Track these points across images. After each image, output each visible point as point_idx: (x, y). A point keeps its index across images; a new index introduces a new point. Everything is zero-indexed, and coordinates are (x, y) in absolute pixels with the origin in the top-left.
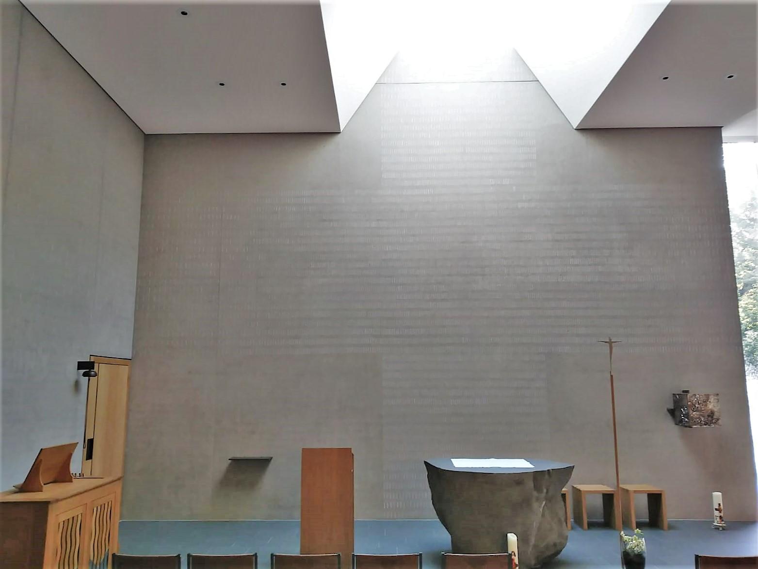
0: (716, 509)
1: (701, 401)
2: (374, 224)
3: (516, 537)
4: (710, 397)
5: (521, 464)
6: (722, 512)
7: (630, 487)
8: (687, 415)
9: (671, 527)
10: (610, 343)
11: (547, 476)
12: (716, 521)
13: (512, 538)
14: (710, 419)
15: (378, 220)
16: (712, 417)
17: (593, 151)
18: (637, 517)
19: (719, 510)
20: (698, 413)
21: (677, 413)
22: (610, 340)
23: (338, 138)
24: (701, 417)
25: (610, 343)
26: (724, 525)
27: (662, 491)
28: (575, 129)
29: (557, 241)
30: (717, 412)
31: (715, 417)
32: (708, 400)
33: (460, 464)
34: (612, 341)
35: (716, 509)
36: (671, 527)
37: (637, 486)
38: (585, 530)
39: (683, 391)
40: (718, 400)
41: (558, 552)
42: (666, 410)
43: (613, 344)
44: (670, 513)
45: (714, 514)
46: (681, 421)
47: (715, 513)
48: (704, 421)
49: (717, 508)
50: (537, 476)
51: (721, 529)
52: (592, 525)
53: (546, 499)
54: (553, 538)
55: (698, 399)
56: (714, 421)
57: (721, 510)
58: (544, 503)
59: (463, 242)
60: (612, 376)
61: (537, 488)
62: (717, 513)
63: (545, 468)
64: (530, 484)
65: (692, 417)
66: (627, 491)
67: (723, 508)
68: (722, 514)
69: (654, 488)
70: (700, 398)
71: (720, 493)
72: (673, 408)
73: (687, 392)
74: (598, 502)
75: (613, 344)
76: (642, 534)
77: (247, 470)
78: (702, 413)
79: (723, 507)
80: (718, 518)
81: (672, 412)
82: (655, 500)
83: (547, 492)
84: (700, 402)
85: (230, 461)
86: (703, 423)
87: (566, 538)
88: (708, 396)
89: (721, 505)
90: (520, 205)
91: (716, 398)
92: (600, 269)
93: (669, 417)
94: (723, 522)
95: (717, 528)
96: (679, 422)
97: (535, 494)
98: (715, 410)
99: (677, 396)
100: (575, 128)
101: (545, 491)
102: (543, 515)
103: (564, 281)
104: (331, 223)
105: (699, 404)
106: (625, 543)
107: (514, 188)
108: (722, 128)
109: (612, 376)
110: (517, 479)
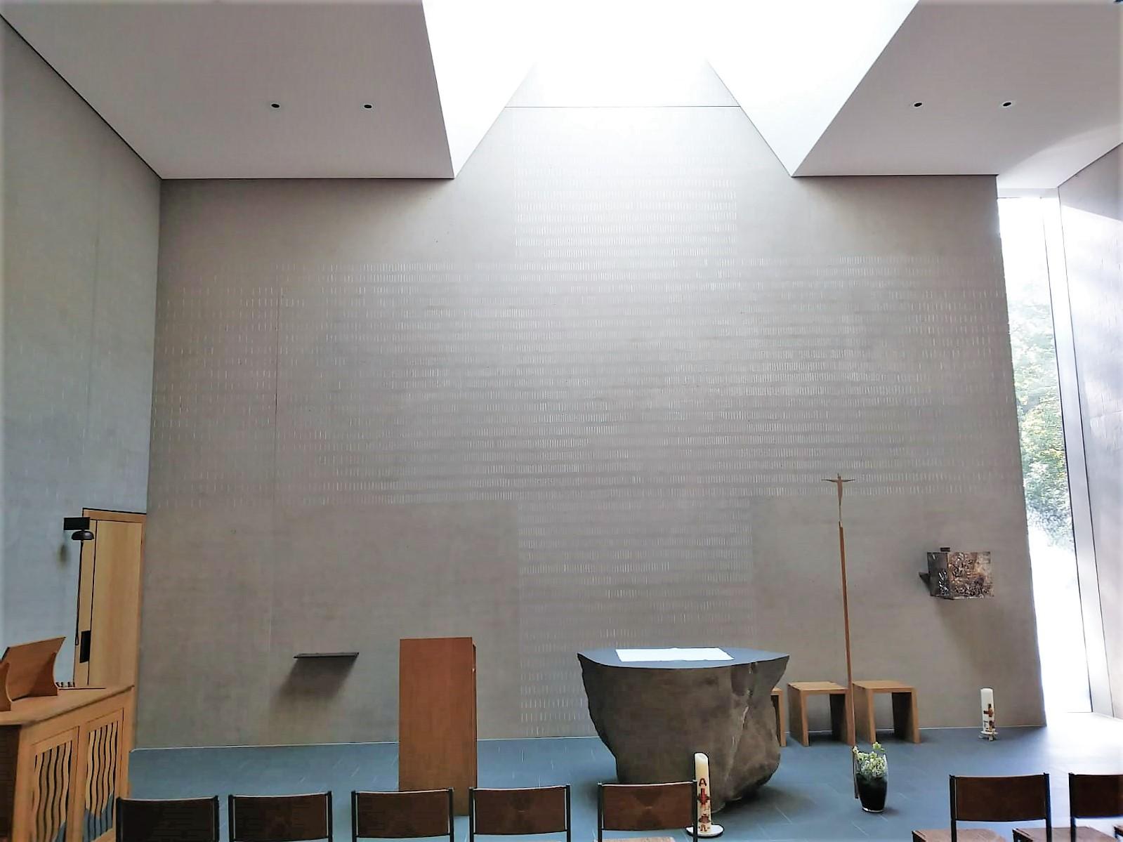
0: (985, 712)
5: (715, 656)
8: (947, 583)
9: (923, 739)
10: (840, 482)
12: (985, 729)
13: (701, 759)
14: (978, 586)
15: (511, 308)
16: (981, 585)
17: (818, 209)
19: (989, 713)
22: (839, 478)
25: (840, 482)
26: (995, 733)
28: (792, 177)
31: (985, 584)
33: (629, 656)
35: (985, 712)
37: (878, 683)
39: (941, 549)
40: (989, 560)
44: (922, 719)
46: (939, 591)
50: (737, 671)
51: (991, 739)
52: (814, 739)
54: (759, 758)
55: (963, 559)
60: (841, 529)
61: (737, 689)
62: (986, 717)
64: (727, 683)
65: (954, 586)
68: (993, 719)
71: (991, 690)
73: (947, 549)
77: (321, 672)
80: (988, 724)
81: (926, 578)
82: (902, 701)
83: (751, 694)
84: (964, 564)
85: (296, 659)
89: (992, 706)
90: (713, 286)
91: (986, 557)
94: (994, 730)
95: (986, 738)
96: (936, 593)
97: (734, 696)
98: (986, 574)
100: (791, 175)
101: (748, 692)
106: (858, 763)
107: (706, 261)
108: (997, 177)
109: (841, 529)
110: (708, 676)
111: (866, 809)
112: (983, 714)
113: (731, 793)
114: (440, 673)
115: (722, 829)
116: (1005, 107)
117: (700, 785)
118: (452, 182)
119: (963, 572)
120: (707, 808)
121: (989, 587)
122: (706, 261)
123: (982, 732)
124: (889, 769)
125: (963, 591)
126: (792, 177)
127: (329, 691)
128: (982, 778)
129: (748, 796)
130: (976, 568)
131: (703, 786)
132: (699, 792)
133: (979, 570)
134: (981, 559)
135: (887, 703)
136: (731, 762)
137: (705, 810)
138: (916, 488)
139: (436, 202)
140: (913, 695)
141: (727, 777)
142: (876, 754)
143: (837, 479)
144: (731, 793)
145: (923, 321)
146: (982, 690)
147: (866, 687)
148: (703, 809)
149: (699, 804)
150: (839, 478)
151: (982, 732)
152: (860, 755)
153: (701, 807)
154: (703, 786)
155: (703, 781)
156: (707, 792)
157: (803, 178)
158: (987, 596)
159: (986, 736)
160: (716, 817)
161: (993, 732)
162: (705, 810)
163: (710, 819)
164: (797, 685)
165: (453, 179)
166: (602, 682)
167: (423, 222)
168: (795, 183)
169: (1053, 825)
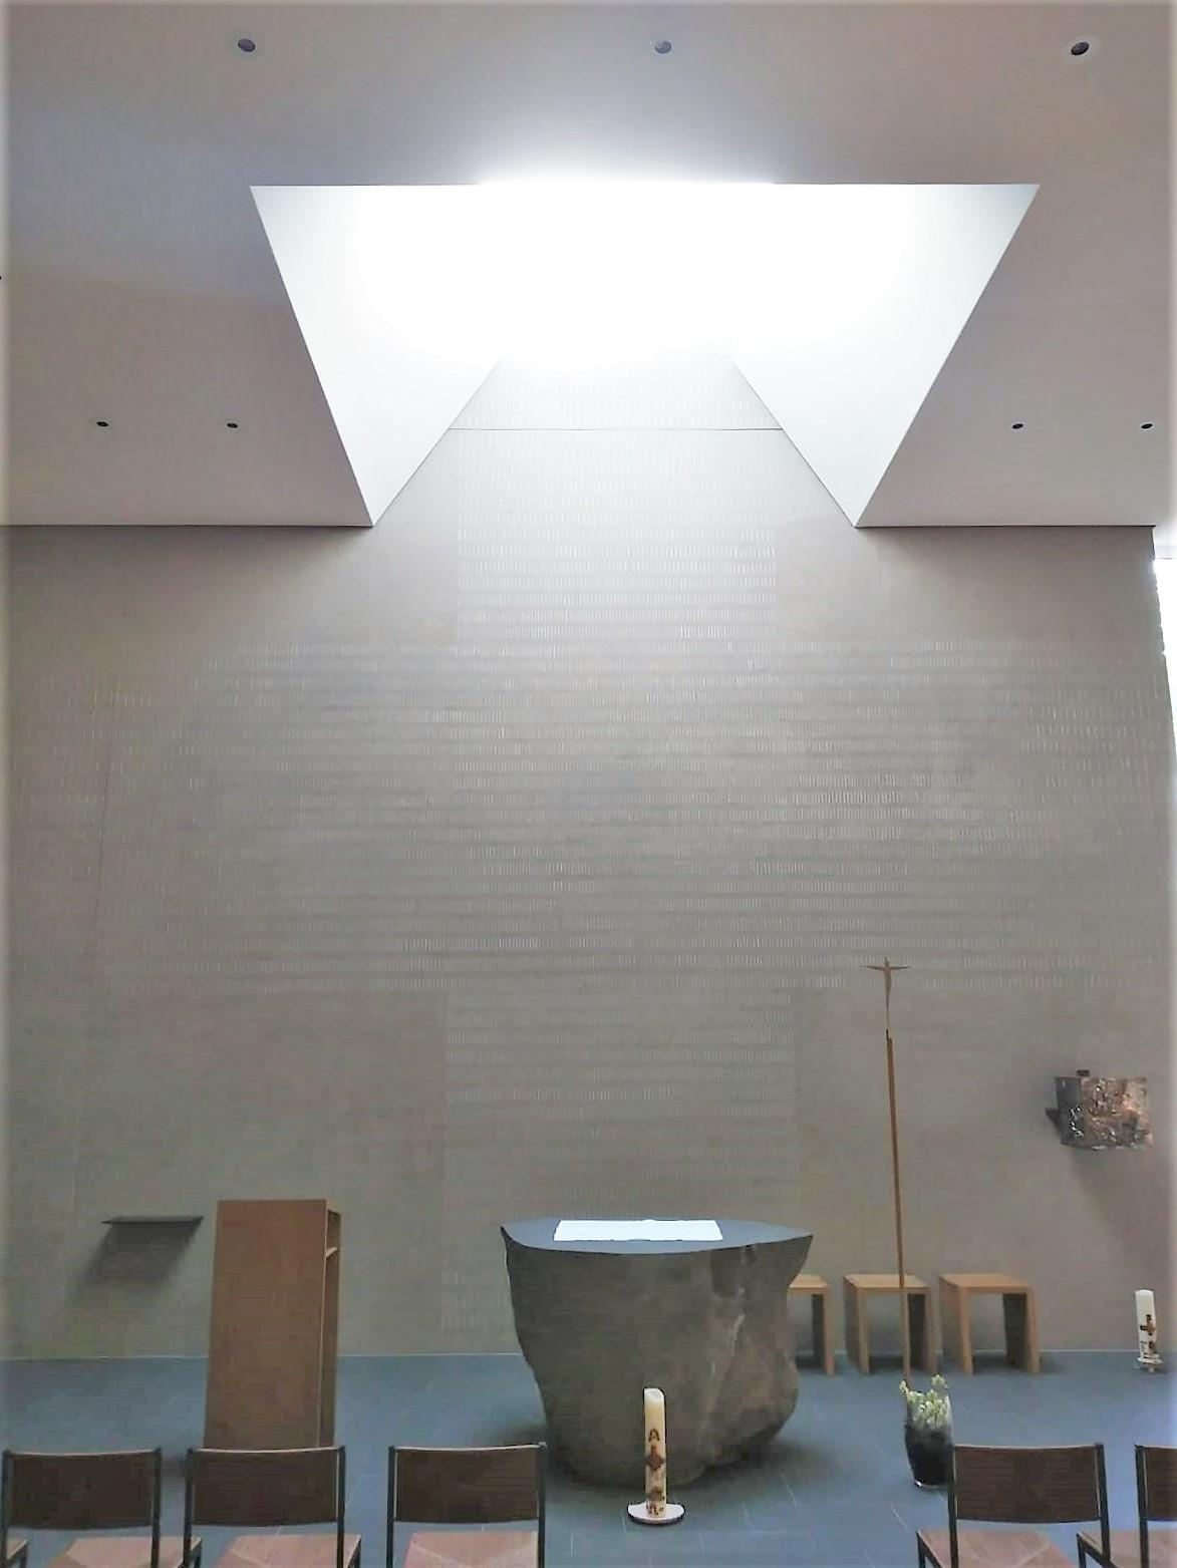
0: (1142, 1328)
1: (1110, 1093)
2: (437, 718)
3: (663, 1396)
4: (1129, 1085)
5: (704, 1232)
6: (1155, 1333)
7: (963, 1280)
8: (1081, 1125)
9: (1048, 1366)
10: (887, 970)
11: (744, 1260)
12: (1142, 1354)
13: (654, 1398)
14: (1129, 1131)
15: (448, 708)
16: (1133, 1128)
17: (891, 573)
18: (975, 1345)
19: (1148, 1329)
20: (1103, 1119)
21: (1064, 1118)
22: (887, 963)
23: (366, 538)
24: (1110, 1128)
25: (887, 970)
26: (1159, 1361)
27: (1025, 1288)
28: (856, 528)
29: (818, 755)
30: (1143, 1115)
31: (1139, 1128)
32: (1124, 1090)
33: (572, 1232)
34: (891, 965)
35: (1142, 1328)
36: (1048, 1366)
37: (980, 1279)
38: (865, 1375)
39: (1079, 1072)
40: (1145, 1091)
41: (775, 1428)
42: (1044, 1112)
43: (892, 972)
44: (1043, 1339)
45: (1138, 1338)
46: (1071, 1135)
47: (1140, 1336)
48: (1116, 1138)
49: (1145, 1324)
50: (719, 1259)
51: (1152, 1370)
52: (982, 1364)
53: (746, 1310)
54: (760, 1395)
55: (1103, 1088)
56: (1136, 1137)
57: (1154, 1329)
58: (741, 1318)
59: (625, 757)
60: (889, 1041)
61: (720, 1286)
62: (1143, 1336)
63: (741, 1240)
64: (705, 1277)
65: (1091, 1128)
66: (954, 1288)
67: (1157, 1324)
68: (1154, 1338)
69: (1012, 1283)
70: (1107, 1087)
71: (1150, 1293)
72: (1056, 1107)
73: (1084, 1073)
74: (899, 1315)
75: (892, 972)
76: (946, 1386)
77: (142, 1245)
78: (1111, 1120)
79: (1157, 1321)
80: (1147, 1346)
81: (1055, 1116)
82: (1016, 1304)
83: (748, 1294)
84: (1106, 1095)
85: (109, 1226)
86: (1115, 1140)
87: (794, 1397)
88: (1123, 1085)
89: (1153, 1318)
90: (740, 681)
91: (1141, 1086)
92: (906, 813)
93: (1050, 1129)
94: (1157, 1356)
95: (1145, 1368)
96: (1068, 1139)
97: (717, 1299)
98: (1140, 1113)
99: (1064, 1084)
100: (854, 524)
101: (742, 1291)
102: (740, 1346)
103: (831, 838)
104: (348, 713)
105: (1105, 1099)
106: (910, 1409)
107: (730, 645)
108: (1154, 530)
109: (889, 1041)
110: (678, 1264)
111: (919, 1483)
112: (1139, 1330)
113: (713, 1451)
114: (289, 1249)
115: (682, 1511)
116: (1144, 430)
117: (650, 1440)
118: (371, 531)
119: (1106, 1109)
120: (660, 1475)
121: (1145, 1132)
122: (730, 645)
123: (1139, 1359)
124: (954, 1417)
125: (1106, 1137)
126: (856, 528)
127: (155, 1277)
128: (65, 1458)
129: (739, 1459)
130: (1125, 1103)
131: (654, 1441)
132: (648, 1450)
133: (1129, 1105)
134: (1133, 1089)
135: (996, 1309)
136: (710, 1404)
137: (658, 1480)
138: (1039, 980)
139: (354, 554)
140: (825, 1298)
141: (704, 1425)
142: (936, 1394)
143: (884, 966)
144: (713, 1451)
145: (1047, 732)
146: (1137, 1293)
147: (959, 1284)
148: (653, 1478)
149: (648, 1469)
150: (887, 963)
151: (1139, 1359)
152: (912, 1395)
153: (650, 1477)
154: (654, 1441)
155: (654, 1434)
156: (662, 1451)
157: (875, 530)
158: (1143, 1147)
159: (1146, 1366)
160: (675, 1491)
161: (1155, 1360)
162: (658, 1480)
163: (664, 1494)
164: (950, 1278)
165: (371, 527)
166: (536, 1273)
167: (326, 587)
168: (862, 539)
169: (181, 1540)
